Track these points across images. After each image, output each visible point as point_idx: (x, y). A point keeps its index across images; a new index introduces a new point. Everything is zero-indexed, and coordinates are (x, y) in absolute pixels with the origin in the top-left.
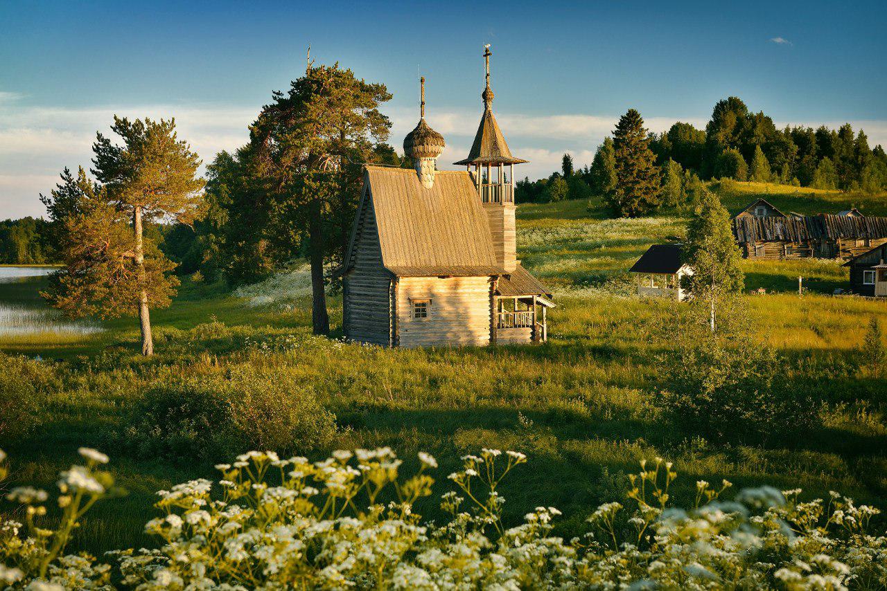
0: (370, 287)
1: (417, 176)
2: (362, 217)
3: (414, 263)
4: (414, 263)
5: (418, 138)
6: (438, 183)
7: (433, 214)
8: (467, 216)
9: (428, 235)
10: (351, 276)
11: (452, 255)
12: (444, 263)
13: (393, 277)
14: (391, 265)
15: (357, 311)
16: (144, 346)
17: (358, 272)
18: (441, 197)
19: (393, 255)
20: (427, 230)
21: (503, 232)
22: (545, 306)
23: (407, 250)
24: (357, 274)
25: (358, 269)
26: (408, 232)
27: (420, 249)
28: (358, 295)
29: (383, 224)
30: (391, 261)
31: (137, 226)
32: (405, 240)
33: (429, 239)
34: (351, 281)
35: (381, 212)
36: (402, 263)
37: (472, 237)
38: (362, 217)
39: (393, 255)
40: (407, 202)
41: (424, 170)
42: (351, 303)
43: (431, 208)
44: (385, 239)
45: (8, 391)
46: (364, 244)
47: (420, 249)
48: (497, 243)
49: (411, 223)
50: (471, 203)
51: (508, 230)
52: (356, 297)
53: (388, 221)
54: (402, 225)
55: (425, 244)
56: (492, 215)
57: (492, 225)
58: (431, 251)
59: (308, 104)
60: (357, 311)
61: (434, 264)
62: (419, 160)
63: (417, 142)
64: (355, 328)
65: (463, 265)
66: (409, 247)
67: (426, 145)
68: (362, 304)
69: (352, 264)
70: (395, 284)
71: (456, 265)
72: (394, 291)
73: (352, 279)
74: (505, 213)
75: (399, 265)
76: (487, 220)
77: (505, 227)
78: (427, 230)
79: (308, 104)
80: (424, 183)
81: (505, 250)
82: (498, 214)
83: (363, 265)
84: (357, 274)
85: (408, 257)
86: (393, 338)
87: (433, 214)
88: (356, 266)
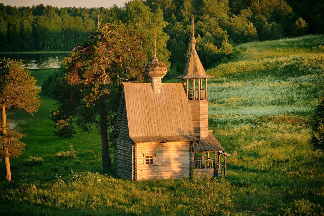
0: (124, 146)
1: (151, 87)
2: (122, 109)
3: (146, 135)
4: (146, 135)
5: (151, 67)
6: (164, 91)
7: (159, 107)
8: (178, 108)
9: (156, 120)
10: (118, 139)
12: (163, 134)
14: (134, 136)
15: (120, 158)
17: (121, 138)
19: (135, 131)
20: (155, 117)
21: (199, 116)
23: (143, 128)
24: (120, 139)
25: (121, 136)
26: (144, 118)
28: (121, 150)
29: (130, 114)
30: (132, 135)
31: (3, 115)
32: (142, 122)
33: (156, 121)
34: (118, 142)
35: (130, 107)
36: (140, 135)
37: (181, 120)
38: (122, 109)
39: (135, 131)
40: (145, 101)
41: (155, 84)
42: (118, 154)
44: (131, 122)
45: (158, 160)
46: (123, 123)
48: (196, 122)
49: (146, 113)
50: (181, 101)
51: (203, 115)
52: (119, 151)
53: (133, 113)
54: (141, 114)
55: (153, 124)
56: (193, 107)
57: (193, 112)
58: (157, 128)
59: (95, 47)
60: (120, 158)
61: (158, 135)
62: (152, 79)
63: (151, 69)
66: (144, 126)
68: (123, 155)
69: (118, 133)
70: (135, 146)
71: (170, 135)
72: (134, 150)
73: (118, 141)
74: (200, 106)
75: (138, 136)
76: (190, 110)
77: (200, 113)
78: (155, 117)
79: (95, 47)
80: (155, 90)
82: (197, 106)
83: (122, 134)
84: (120, 139)
85: (143, 132)
86: (134, 175)
87: (159, 107)
88: (120, 134)
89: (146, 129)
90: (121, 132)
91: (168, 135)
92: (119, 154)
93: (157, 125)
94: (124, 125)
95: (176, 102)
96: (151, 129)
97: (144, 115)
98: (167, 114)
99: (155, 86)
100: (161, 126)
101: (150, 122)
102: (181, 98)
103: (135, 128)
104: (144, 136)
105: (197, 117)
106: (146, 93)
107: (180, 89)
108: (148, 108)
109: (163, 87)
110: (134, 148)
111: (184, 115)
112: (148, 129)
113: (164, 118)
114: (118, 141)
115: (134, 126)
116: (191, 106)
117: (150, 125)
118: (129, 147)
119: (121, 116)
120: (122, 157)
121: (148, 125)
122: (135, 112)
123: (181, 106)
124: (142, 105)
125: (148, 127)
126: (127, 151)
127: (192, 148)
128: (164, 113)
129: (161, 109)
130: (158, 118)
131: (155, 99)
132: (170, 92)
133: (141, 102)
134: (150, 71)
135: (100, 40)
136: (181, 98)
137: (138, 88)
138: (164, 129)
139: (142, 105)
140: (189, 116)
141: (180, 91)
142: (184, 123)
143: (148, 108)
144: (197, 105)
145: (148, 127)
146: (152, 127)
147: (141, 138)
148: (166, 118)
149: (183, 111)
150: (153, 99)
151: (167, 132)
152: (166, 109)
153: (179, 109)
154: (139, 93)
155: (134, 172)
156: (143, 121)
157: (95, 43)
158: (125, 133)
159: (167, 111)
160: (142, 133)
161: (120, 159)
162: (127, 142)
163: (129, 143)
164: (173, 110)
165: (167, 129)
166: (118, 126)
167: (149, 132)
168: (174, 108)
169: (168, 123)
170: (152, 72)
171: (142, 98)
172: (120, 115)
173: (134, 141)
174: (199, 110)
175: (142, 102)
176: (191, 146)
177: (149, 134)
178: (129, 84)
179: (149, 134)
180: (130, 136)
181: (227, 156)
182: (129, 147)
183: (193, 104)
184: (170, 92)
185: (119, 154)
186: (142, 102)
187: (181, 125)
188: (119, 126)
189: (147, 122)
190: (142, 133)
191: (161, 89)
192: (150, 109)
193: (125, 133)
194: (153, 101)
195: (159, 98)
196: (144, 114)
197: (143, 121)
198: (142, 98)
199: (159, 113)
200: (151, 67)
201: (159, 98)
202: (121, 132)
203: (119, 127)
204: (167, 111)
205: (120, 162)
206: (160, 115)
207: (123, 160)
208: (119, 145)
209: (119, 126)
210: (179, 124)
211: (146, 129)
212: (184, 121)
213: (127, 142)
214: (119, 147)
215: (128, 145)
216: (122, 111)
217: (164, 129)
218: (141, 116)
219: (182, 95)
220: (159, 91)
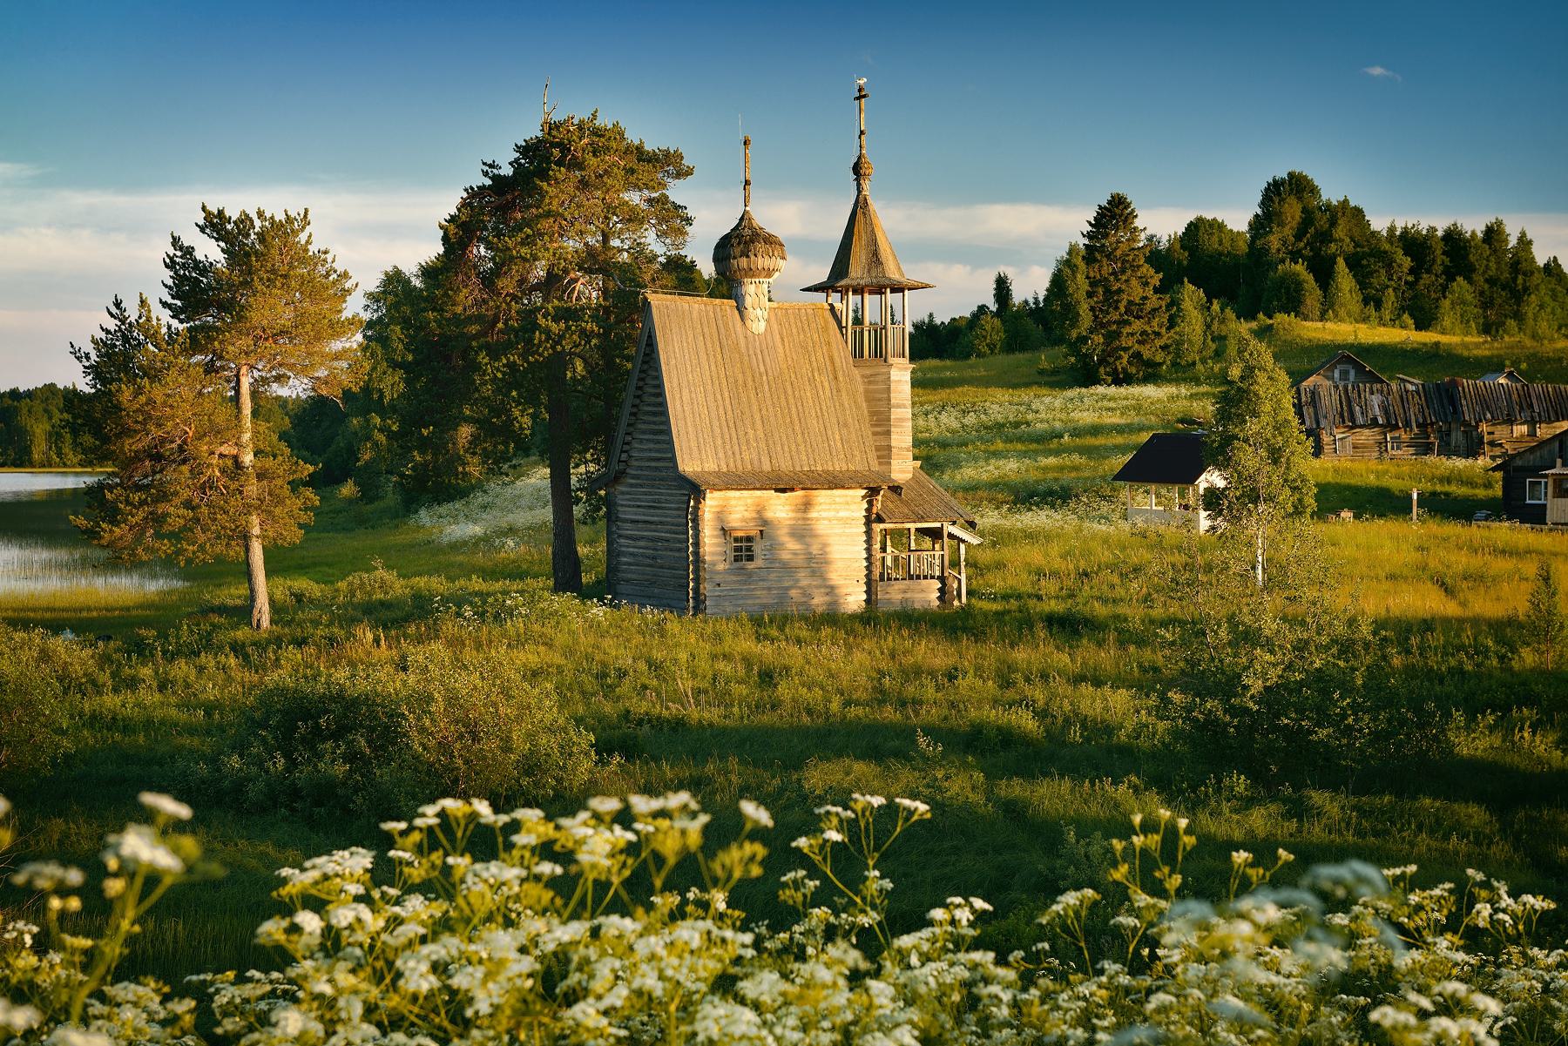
3: (732, 465)
4: (732, 465)
5: (739, 244)
6: (775, 327)
8: (824, 381)
9: (757, 417)
11: (798, 452)
13: (694, 490)
16: (255, 612)
18: (780, 350)
20: (755, 407)
21: (889, 411)
22: (964, 541)
23: (719, 442)
26: (721, 411)
27: (743, 441)
28: (633, 521)
30: (688, 465)
33: (759, 422)
36: (710, 466)
37: (834, 420)
38: (641, 384)
40: (719, 357)
41: (749, 301)
43: (762, 369)
46: (644, 432)
47: (743, 441)
49: (726, 394)
53: (685, 392)
54: (711, 398)
55: (751, 432)
56: (869, 380)
57: (870, 398)
58: (763, 445)
61: (767, 467)
62: (740, 284)
63: (737, 251)
64: (627, 581)
65: (819, 468)
67: (753, 257)
68: (642, 538)
69: (622, 466)
70: (698, 502)
73: (623, 493)
76: (861, 388)
78: (755, 407)
80: (748, 323)
81: (893, 444)
82: (880, 378)
83: (641, 468)
84: (632, 485)
85: (721, 455)
88: (628, 471)
89: (728, 447)
90: (636, 463)
91: (798, 469)
92: (627, 537)
93: (762, 436)
94: (646, 437)
95: (815, 364)
96: (744, 448)
97: (720, 402)
98: (792, 401)
99: (750, 309)
100: (777, 438)
101: (739, 424)
102: (829, 351)
103: (693, 444)
104: (725, 470)
105: (881, 413)
106: (722, 331)
107: (826, 322)
108: (731, 380)
109: (772, 314)
110: (696, 508)
111: (842, 405)
112: (736, 448)
113: (782, 413)
114: (623, 493)
115: (692, 436)
116: (863, 376)
117: (741, 433)
118: (670, 509)
119: (635, 410)
120: (642, 543)
121: (734, 435)
122: (691, 392)
123: (831, 376)
124: (713, 368)
125: (735, 439)
126: (661, 523)
127: (875, 511)
128: (783, 397)
129: (772, 383)
130: (764, 412)
131: (751, 352)
132: (794, 331)
133: (708, 360)
134: (735, 258)
135: (559, 163)
136: (829, 351)
137: (695, 314)
138: (786, 448)
139: (713, 368)
140: (858, 407)
141: (826, 329)
142: (844, 431)
143: (731, 380)
144: (883, 374)
145: (735, 439)
146: (748, 442)
147: (718, 474)
148: (790, 412)
149: (838, 391)
150: (743, 350)
151: (795, 457)
152: (788, 385)
153: (826, 384)
154: (700, 331)
155: (696, 590)
156: (719, 419)
157: (544, 175)
158: (653, 464)
159: (790, 391)
160: (719, 459)
161: (632, 554)
162: (662, 494)
163: (672, 495)
164: (808, 388)
165: (793, 447)
166: (625, 443)
167: (738, 457)
168: (812, 380)
169: (797, 428)
170: (743, 262)
171: (709, 345)
172: (633, 406)
173: (698, 481)
174: (889, 389)
175: (712, 358)
176: (870, 503)
177: (739, 463)
178: (667, 300)
179: (739, 463)
180: (680, 469)
181: (969, 546)
182: (670, 509)
183: (868, 372)
184: (794, 331)
185: (627, 537)
186: (712, 358)
187: (837, 437)
188: (628, 444)
189: (731, 425)
190: (719, 459)
191: (768, 321)
192: (736, 381)
193: (653, 464)
194: (746, 358)
195: (764, 347)
196: (719, 397)
197: (719, 419)
198: (709, 345)
199: (768, 395)
200: (739, 244)
201: (764, 347)
202: (636, 463)
203: (626, 447)
204: (790, 391)
205: (630, 564)
206: (769, 402)
207: (643, 555)
208: (629, 506)
209: (628, 444)
210: (830, 433)
211: (728, 447)
212: (846, 425)
213: (662, 494)
214: (627, 513)
215: (667, 501)
216: (640, 393)
217: (786, 448)
218: (712, 405)
219: (833, 340)
220: (763, 325)
